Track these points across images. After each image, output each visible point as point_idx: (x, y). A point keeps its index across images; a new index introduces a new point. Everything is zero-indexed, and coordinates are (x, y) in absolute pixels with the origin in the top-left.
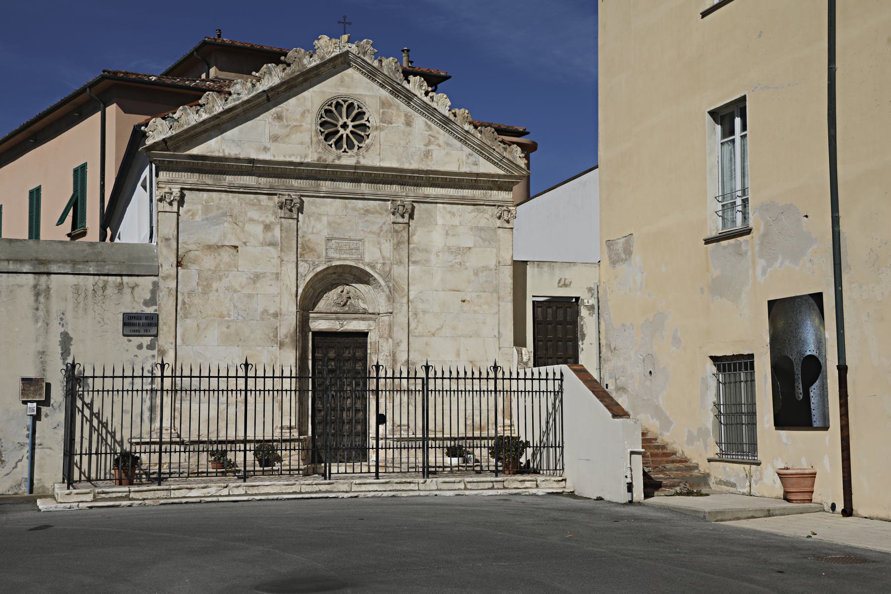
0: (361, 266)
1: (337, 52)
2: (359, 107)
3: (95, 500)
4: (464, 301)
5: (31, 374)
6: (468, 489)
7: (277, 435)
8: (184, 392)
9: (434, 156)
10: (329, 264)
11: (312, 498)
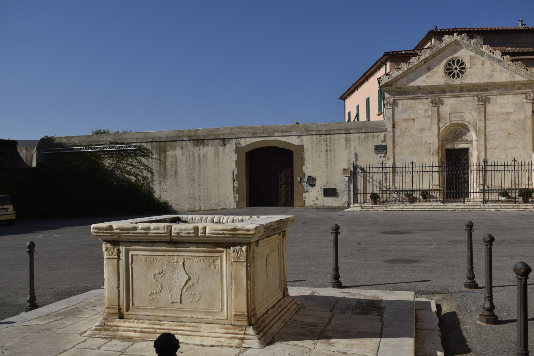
0: (464, 123)
1: (452, 40)
2: (462, 61)
3: (362, 209)
4: (509, 134)
5: (346, 167)
6: (502, 208)
7: (431, 188)
8: (390, 173)
9: (495, 76)
10: (451, 123)
11: (437, 210)
